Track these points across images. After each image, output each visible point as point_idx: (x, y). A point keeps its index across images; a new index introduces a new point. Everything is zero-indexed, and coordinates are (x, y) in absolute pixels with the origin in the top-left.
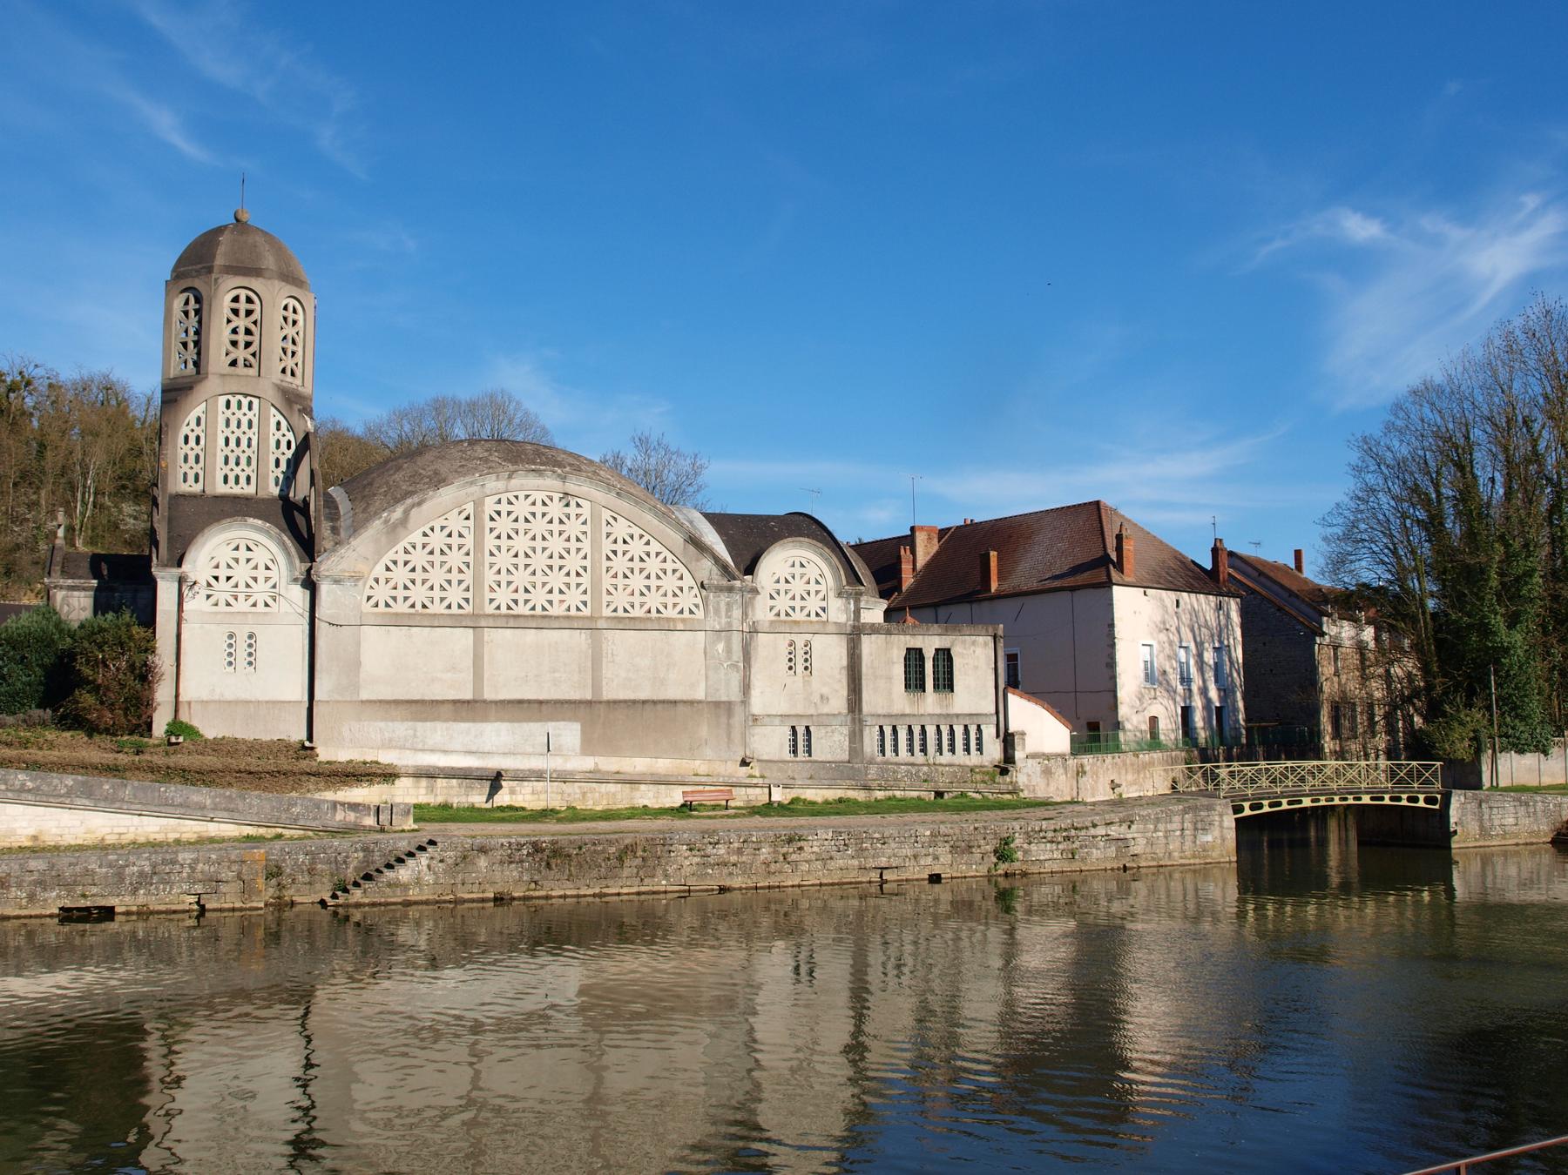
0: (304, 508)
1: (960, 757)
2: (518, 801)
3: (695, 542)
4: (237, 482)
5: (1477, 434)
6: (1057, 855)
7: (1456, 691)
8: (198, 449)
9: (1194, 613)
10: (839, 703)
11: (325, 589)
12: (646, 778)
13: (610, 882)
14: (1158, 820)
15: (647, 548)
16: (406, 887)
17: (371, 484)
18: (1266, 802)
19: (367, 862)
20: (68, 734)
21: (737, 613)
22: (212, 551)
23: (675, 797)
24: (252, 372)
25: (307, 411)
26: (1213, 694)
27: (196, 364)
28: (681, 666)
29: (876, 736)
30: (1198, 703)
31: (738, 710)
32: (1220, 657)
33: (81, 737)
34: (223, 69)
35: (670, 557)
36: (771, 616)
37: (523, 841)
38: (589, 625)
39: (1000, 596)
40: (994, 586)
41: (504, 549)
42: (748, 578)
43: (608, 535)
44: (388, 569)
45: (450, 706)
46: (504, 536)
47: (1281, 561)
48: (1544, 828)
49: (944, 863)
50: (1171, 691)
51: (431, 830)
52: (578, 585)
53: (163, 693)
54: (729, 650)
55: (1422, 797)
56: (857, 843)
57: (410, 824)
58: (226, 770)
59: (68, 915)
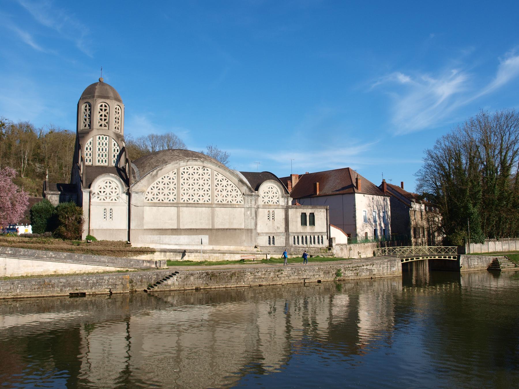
0: (124, 169)
1: (317, 245)
2: (190, 259)
3: (241, 181)
4: (102, 162)
5: (462, 151)
6: (353, 274)
7: (458, 225)
8: (90, 152)
9: (378, 201)
10: (282, 229)
11: (133, 195)
12: (230, 252)
13: (228, 284)
14: (381, 264)
15: (227, 183)
16: (170, 286)
17: (143, 163)
18: (410, 259)
19: (157, 278)
20: (57, 240)
21: (253, 202)
22: (100, 183)
23: (238, 257)
24: (107, 128)
25: (123, 140)
26: (383, 225)
27: (89, 126)
28: (237, 218)
29: (293, 239)
30: (378, 228)
31: (254, 231)
32: (384, 214)
33: (61, 240)
34: (47, 22)
35: (234, 186)
36: (263, 203)
37: (203, 272)
38: (210, 206)
39: (319, 196)
40: (318, 193)
41: (186, 183)
42: (256, 192)
43: (216, 179)
44: (152, 189)
45: (170, 231)
46: (186, 179)
47: (397, 185)
48: (485, 265)
49: (322, 277)
50: (371, 224)
51: (173, 269)
52: (207, 194)
53: (85, 227)
54: (251, 214)
55: (452, 257)
56: (298, 271)
57: (166, 267)
58: (105, 250)
59: (72, 295)
